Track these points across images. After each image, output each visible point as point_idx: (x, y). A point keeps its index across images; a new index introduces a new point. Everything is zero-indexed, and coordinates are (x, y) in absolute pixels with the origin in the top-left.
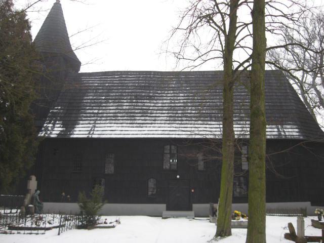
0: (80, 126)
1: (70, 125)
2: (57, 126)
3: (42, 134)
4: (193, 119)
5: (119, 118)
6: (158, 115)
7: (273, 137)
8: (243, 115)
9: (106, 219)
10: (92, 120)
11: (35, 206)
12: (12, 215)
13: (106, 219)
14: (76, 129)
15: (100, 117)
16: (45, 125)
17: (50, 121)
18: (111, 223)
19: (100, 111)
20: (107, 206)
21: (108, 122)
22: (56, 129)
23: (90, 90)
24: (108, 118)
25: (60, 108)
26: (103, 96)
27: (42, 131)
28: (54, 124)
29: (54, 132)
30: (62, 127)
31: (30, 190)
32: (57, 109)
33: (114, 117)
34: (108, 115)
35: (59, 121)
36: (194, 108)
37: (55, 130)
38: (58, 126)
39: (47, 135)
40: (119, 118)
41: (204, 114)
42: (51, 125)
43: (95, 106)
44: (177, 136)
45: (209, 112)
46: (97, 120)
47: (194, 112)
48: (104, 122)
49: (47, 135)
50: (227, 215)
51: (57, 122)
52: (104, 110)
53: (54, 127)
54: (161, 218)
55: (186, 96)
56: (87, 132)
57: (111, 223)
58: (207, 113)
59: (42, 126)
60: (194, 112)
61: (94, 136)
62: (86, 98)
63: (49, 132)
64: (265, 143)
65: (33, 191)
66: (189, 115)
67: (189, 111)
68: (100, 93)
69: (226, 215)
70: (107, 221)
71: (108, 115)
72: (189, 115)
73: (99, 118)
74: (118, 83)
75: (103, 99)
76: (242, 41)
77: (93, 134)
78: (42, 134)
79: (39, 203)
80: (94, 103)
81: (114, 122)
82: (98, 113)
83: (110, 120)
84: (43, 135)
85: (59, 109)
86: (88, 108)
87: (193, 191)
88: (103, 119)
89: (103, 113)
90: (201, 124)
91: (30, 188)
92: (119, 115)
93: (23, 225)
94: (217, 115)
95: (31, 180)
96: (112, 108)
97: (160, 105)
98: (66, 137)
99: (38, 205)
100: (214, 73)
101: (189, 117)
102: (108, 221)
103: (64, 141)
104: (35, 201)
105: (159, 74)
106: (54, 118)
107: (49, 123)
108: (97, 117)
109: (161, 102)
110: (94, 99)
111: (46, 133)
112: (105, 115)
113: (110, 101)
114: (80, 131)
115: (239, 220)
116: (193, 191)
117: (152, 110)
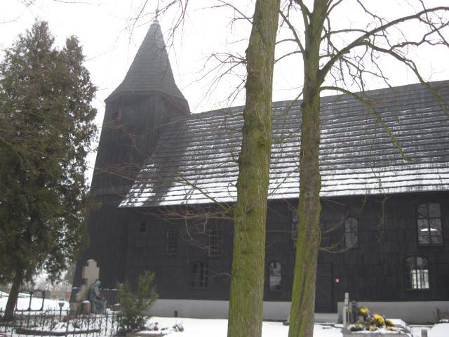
0: (176, 188)
1: (161, 190)
2: (146, 190)
3: (124, 204)
4: (339, 166)
5: (230, 174)
6: (284, 165)
7: (414, 189)
8: (422, 154)
9: (157, 324)
10: (192, 179)
11: (91, 302)
12: (32, 313)
13: (157, 324)
14: (169, 194)
15: (204, 174)
16: (132, 190)
17: (139, 184)
18: (163, 329)
19: (205, 166)
20: (161, 303)
21: (213, 180)
22: (143, 195)
23: (195, 137)
24: (214, 175)
25: (153, 165)
26: (211, 145)
27: (125, 199)
28: (142, 189)
29: (140, 200)
30: (153, 192)
31: (87, 279)
32: (150, 167)
33: (222, 172)
34: (215, 170)
35: (149, 183)
36: (341, 150)
37: (141, 197)
38: (148, 190)
39: (130, 204)
40: (230, 174)
41: (357, 157)
42: (138, 190)
43: (199, 160)
44: (352, 193)
45: (364, 153)
46: (199, 179)
47: (340, 155)
48: (341, 172)
49: (130, 204)
50: (303, 322)
51: (147, 185)
52: (211, 163)
53: (141, 192)
54: (282, 323)
55: (332, 133)
56: (183, 197)
57: (163, 329)
58: (362, 156)
59: (127, 192)
60: (340, 155)
61: (191, 202)
62: (188, 148)
63: (134, 200)
64: (264, 207)
65: (89, 283)
66: (332, 161)
67: (333, 155)
68: (209, 140)
69: (301, 324)
70: (158, 326)
71: (215, 170)
72: (332, 161)
73: (201, 176)
74: (235, 124)
75: (211, 149)
76: (344, 33)
77: (190, 199)
78: (124, 204)
79: (98, 298)
80: (199, 154)
81: (221, 179)
82: (202, 169)
83: (216, 177)
84: (125, 204)
85: (152, 168)
86: (189, 162)
87: (337, 281)
88: (208, 176)
89: (208, 168)
90: (349, 174)
91: (86, 277)
92: (230, 169)
93: (39, 329)
94: (377, 158)
95: (88, 265)
96: (221, 160)
97: (290, 149)
98: (155, 205)
99: (95, 300)
100: (378, 93)
101: (332, 164)
102: (159, 327)
103: (152, 209)
104: (92, 296)
105: (342, 98)
106: (145, 180)
107: (137, 188)
108: (199, 174)
109: (292, 144)
110: (199, 150)
111: (130, 202)
112: (211, 171)
113: (221, 150)
114: (174, 197)
115: (377, 332)
116: (337, 281)
117: (278, 158)
